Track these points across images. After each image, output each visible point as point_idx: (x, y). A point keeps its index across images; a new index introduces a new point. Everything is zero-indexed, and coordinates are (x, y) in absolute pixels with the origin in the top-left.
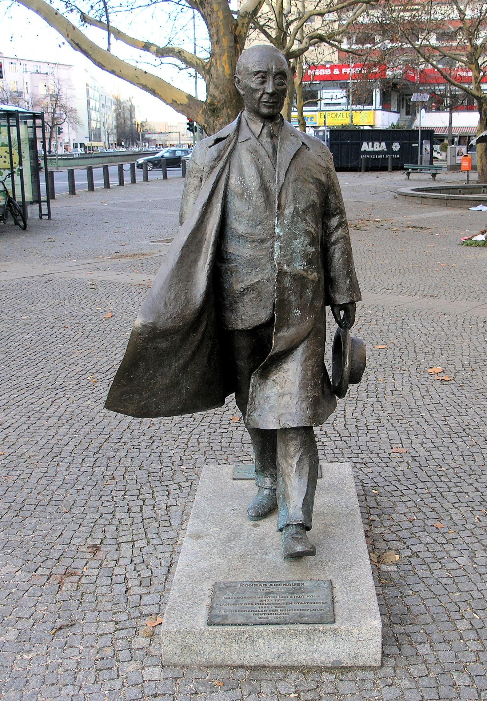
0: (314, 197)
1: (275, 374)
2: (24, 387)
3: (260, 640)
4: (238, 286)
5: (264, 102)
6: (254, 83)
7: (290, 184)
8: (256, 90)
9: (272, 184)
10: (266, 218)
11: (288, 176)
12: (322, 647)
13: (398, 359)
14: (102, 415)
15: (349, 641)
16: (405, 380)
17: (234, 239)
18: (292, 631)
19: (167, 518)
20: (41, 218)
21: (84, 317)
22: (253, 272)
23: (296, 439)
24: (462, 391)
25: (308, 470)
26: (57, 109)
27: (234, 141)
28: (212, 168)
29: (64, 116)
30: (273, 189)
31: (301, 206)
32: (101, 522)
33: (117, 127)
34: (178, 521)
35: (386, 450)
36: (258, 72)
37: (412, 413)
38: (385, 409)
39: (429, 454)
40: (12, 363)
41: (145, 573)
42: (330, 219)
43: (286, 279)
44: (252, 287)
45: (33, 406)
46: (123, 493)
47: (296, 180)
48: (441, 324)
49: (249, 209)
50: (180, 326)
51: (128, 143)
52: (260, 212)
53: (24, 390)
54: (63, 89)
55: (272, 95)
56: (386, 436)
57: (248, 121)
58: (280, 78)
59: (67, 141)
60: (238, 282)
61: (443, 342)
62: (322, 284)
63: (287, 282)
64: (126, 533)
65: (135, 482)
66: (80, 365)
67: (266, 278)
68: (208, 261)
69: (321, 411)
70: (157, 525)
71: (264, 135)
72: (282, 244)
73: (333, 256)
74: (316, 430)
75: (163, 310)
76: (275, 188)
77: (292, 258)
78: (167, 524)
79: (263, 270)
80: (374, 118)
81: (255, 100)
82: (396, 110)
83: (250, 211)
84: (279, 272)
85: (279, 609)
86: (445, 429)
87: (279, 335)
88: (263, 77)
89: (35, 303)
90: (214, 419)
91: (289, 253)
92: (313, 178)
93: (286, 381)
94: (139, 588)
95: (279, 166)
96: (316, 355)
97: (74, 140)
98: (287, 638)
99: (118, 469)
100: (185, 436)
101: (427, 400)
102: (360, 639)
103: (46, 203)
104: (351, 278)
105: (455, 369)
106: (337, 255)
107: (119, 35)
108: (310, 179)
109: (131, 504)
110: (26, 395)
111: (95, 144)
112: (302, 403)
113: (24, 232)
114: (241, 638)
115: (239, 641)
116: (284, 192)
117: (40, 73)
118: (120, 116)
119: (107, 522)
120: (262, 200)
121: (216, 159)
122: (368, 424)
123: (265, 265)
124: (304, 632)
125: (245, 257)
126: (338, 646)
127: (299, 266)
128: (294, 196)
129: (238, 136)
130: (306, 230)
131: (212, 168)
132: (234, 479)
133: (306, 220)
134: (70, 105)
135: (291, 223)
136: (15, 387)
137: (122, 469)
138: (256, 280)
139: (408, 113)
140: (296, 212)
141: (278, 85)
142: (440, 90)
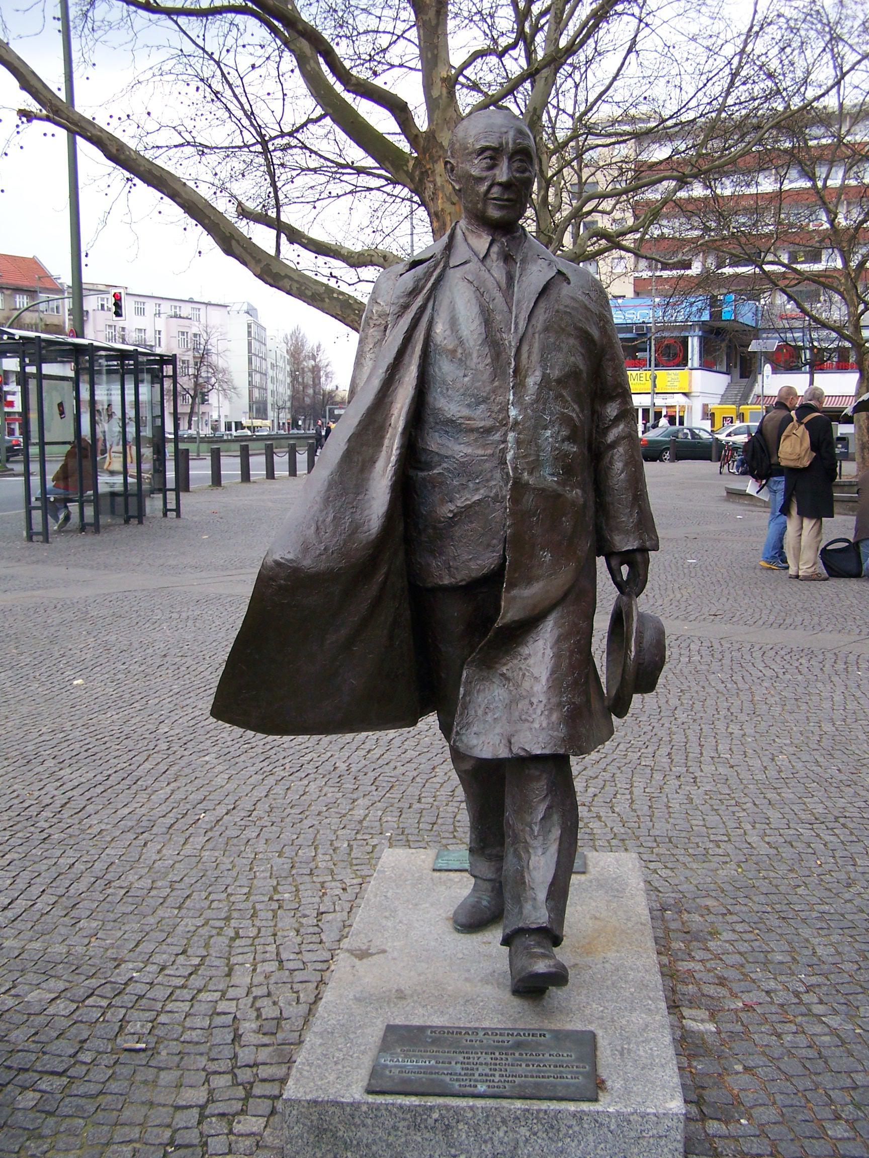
0: (578, 361)
1: (505, 664)
2: (107, 734)
3: (461, 1126)
4: (444, 508)
5: (494, 199)
6: (476, 168)
7: (537, 336)
8: (480, 180)
9: (504, 336)
10: (494, 391)
11: (533, 322)
12: (573, 1145)
13: (723, 712)
14: (227, 776)
15: (624, 1137)
16: (734, 742)
17: (438, 427)
18: (519, 1112)
19: (316, 929)
20: (165, 515)
21: (214, 644)
22: (471, 485)
23: (538, 779)
24: (832, 761)
25: (558, 836)
26: (204, 369)
27: (442, 265)
28: (405, 307)
29: (213, 380)
30: (506, 342)
31: (556, 373)
32: (204, 931)
33: (293, 398)
34: (335, 936)
35: (700, 844)
36: (483, 150)
37: (746, 791)
38: (699, 784)
39: (774, 852)
40: (92, 703)
41: (269, 1011)
42: (605, 404)
43: (526, 497)
44: (467, 512)
45: (116, 761)
46: (246, 890)
47: (546, 329)
48: (797, 664)
49: (465, 376)
50: (340, 569)
51: (307, 422)
52: (484, 382)
53: (106, 739)
54: (213, 341)
55: (506, 186)
56: (701, 823)
57: (467, 233)
58: (521, 161)
59: (215, 417)
60: (443, 502)
61: (800, 690)
62: (591, 512)
63: (529, 500)
64: (246, 949)
65: (268, 874)
66: (200, 707)
67: (492, 495)
68: (393, 459)
69: (584, 731)
70: (299, 939)
71: (494, 256)
72: (521, 436)
73: (609, 468)
74: (575, 764)
75: (313, 539)
76: (510, 339)
77: (538, 460)
78: (315, 939)
79: (488, 481)
80: (690, 381)
81: (478, 194)
82: (724, 370)
83: (466, 379)
84: (515, 483)
85: (497, 1073)
86: (803, 817)
87: (514, 592)
88: (491, 158)
89: (140, 624)
90: (410, 789)
91: (532, 452)
92: (577, 328)
93: (524, 675)
94: (256, 1035)
95: (517, 305)
96: (578, 632)
97: (226, 416)
98: (510, 1124)
99: (243, 855)
100: (359, 813)
101: (771, 773)
102: (644, 1134)
103: (174, 493)
104: (640, 506)
105: (821, 730)
106: (618, 465)
107: (295, 236)
108: (570, 330)
109: (258, 906)
110: (108, 745)
111: (257, 422)
112: (550, 714)
113: (133, 528)
114: (426, 1120)
115: (422, 1126)
116: (525, 348)
117: (180, 317)
118: (298, 381)
119: (214, 932)
120: (489, 360)
121: (410, 293)
122: (670, 805)
123: (491, 471)
124: (541, 1115)
125: (457, 457)
126: (602, 1146)
127: (548, 477)
128: (542, 356)
129: (448, 257)
130: (563, 413)
131: (405, 307)
132: (434, 870)
133: (562, 396)
134: (221, 363)
135: (537, 401)
136: (91, 735)
137: (249, 855)
138: (477, 497)
139: (742, 376)
140: (545, 383)
141: (517, 171)
142: (795, 340)
